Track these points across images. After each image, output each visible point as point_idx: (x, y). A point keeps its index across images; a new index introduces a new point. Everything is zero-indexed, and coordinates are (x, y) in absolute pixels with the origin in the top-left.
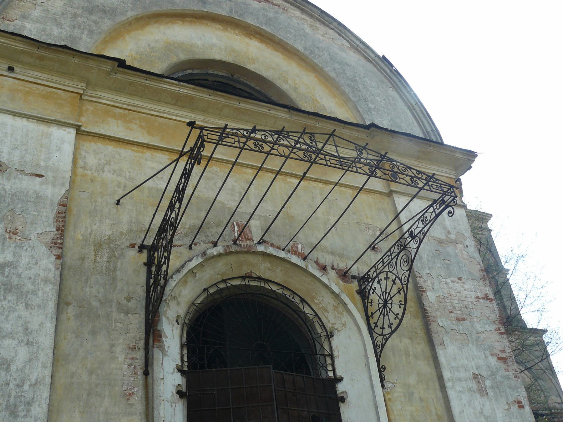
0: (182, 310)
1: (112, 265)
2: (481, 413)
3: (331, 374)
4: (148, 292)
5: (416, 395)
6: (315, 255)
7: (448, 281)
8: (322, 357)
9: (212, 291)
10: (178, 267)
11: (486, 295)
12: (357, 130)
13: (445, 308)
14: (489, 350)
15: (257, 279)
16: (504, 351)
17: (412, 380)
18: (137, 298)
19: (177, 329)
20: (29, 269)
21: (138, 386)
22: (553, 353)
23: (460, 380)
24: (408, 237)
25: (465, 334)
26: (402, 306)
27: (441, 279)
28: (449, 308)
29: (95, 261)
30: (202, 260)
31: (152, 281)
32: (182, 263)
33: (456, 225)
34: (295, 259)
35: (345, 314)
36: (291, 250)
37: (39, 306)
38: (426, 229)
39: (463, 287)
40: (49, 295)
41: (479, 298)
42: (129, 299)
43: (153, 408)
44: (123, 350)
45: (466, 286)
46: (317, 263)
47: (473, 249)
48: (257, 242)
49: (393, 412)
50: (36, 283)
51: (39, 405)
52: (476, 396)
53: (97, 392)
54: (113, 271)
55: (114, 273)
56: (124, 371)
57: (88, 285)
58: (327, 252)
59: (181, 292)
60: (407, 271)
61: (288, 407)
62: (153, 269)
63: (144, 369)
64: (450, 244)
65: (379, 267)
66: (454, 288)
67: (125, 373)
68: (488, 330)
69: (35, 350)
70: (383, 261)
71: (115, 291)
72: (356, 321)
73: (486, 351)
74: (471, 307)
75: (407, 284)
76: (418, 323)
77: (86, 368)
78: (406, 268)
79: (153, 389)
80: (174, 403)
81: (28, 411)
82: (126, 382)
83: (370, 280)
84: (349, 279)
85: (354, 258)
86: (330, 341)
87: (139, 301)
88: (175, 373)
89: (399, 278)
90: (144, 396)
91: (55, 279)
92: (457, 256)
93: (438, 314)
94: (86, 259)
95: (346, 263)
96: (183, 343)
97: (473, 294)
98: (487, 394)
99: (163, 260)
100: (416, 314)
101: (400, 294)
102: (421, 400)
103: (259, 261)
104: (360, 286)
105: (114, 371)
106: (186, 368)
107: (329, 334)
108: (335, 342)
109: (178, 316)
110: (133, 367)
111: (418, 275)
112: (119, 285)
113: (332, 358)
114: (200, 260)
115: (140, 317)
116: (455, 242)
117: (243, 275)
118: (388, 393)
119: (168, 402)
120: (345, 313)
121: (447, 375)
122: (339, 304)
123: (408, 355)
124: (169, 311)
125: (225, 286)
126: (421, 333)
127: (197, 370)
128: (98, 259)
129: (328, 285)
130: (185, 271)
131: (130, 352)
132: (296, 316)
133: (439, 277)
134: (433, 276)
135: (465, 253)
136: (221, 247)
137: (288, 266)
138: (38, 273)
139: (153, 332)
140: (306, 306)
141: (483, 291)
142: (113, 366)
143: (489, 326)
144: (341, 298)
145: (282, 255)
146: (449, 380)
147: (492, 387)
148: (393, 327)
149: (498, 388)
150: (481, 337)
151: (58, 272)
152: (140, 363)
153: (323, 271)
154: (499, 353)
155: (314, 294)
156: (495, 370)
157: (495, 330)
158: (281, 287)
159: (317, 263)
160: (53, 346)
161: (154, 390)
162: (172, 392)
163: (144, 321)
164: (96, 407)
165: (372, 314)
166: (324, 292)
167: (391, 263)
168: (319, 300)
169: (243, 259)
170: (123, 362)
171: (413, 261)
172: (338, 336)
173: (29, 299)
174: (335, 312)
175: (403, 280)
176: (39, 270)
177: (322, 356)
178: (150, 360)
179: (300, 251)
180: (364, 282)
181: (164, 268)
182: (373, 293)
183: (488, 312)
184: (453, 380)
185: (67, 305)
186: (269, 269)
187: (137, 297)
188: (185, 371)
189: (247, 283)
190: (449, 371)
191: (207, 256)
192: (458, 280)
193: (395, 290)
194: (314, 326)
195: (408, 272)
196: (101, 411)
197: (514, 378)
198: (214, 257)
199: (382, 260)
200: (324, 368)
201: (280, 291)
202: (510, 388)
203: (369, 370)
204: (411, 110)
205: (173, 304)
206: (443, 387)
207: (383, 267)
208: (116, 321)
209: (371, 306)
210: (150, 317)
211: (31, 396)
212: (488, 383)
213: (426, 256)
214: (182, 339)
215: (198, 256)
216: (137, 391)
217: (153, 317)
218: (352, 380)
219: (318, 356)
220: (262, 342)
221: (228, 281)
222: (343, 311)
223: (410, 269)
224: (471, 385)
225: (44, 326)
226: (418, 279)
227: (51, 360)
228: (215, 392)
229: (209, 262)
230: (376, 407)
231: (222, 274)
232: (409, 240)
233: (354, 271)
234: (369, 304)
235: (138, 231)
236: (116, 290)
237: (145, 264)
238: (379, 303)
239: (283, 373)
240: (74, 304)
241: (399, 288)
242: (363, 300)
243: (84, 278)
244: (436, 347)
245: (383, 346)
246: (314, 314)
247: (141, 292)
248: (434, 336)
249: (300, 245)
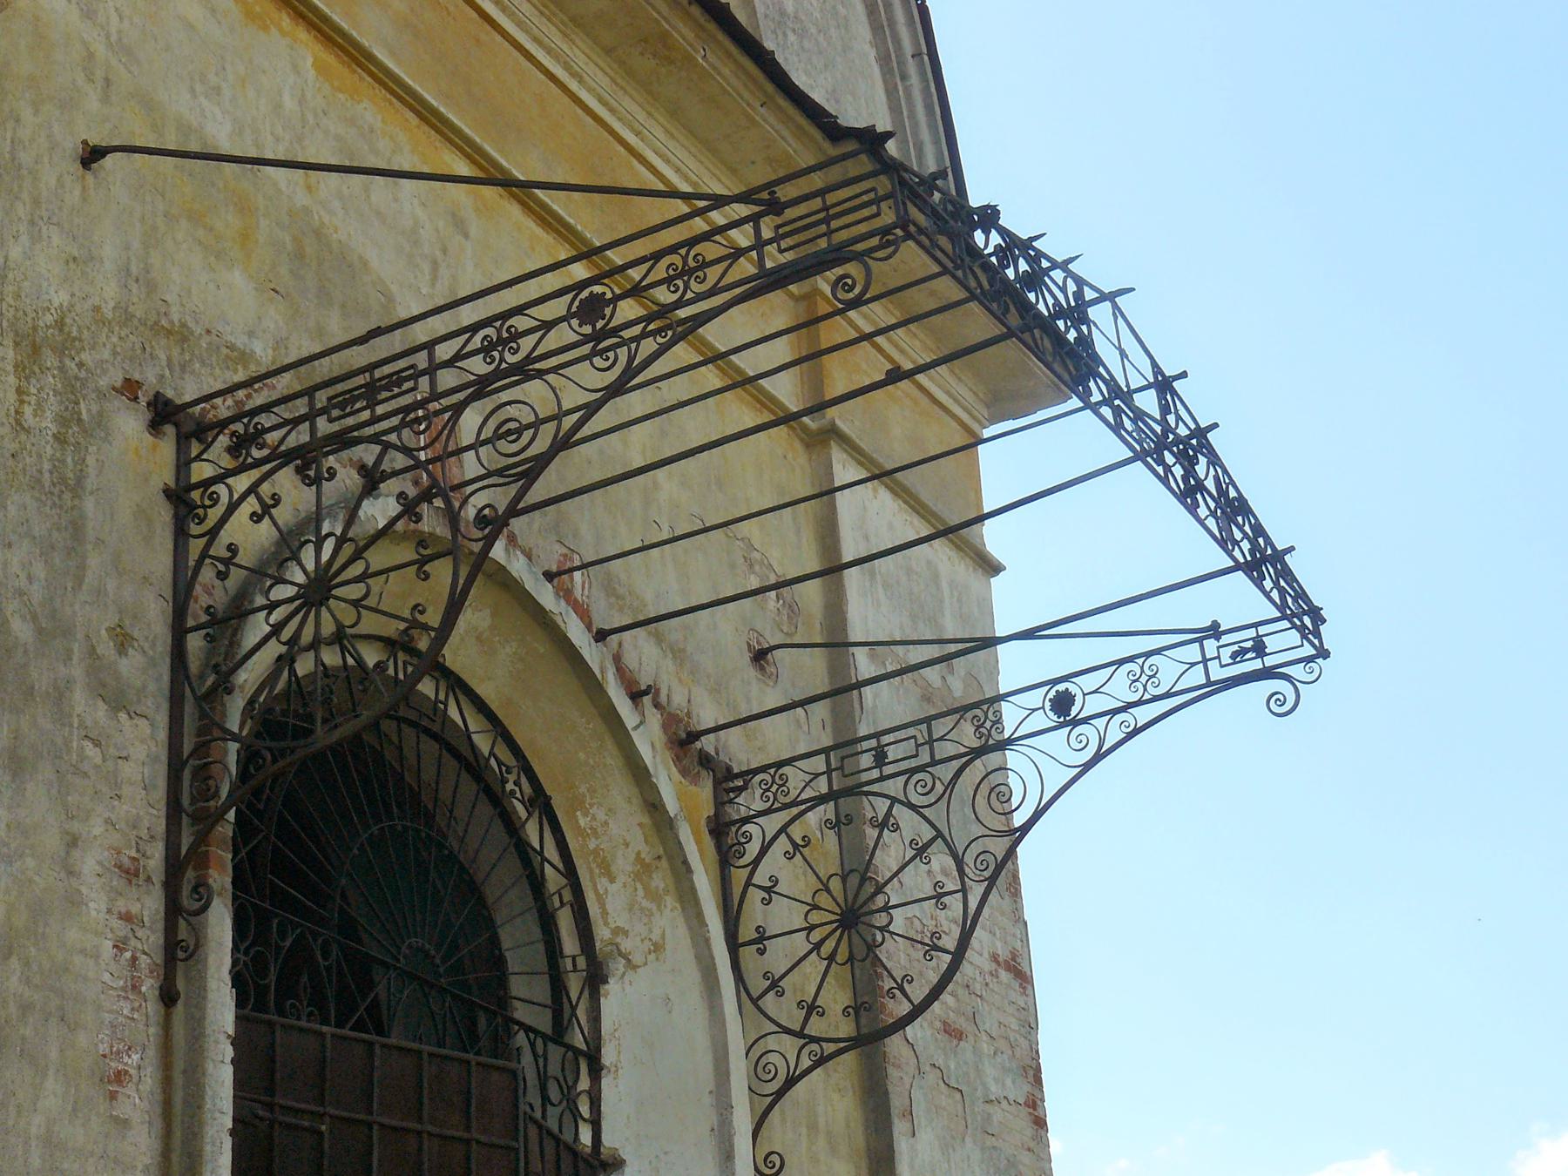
12: (799, 127)
18: (146, 646)
34: (577, 633)
35: (669, 907)
42: (123, 640)
63: (162, 972)
71: (80, 586)
72: (710, 949)
90: (159, 1097)
95: (690, 691)
110: (128, 955)
113: (596, 1070)
120: (670, 901)
122: (659, 857)
129: (651, 770)
137: (542, 646)
144: (677, 837)
155: (583, 789)
166: (620, 792)
168: (594, 818)
172: (627, 987)
174: (639, 886)
196: (34, 1130)
204: (891, 71)
222: (667, 892)
228: (323, 1128)
235: (149, 323)
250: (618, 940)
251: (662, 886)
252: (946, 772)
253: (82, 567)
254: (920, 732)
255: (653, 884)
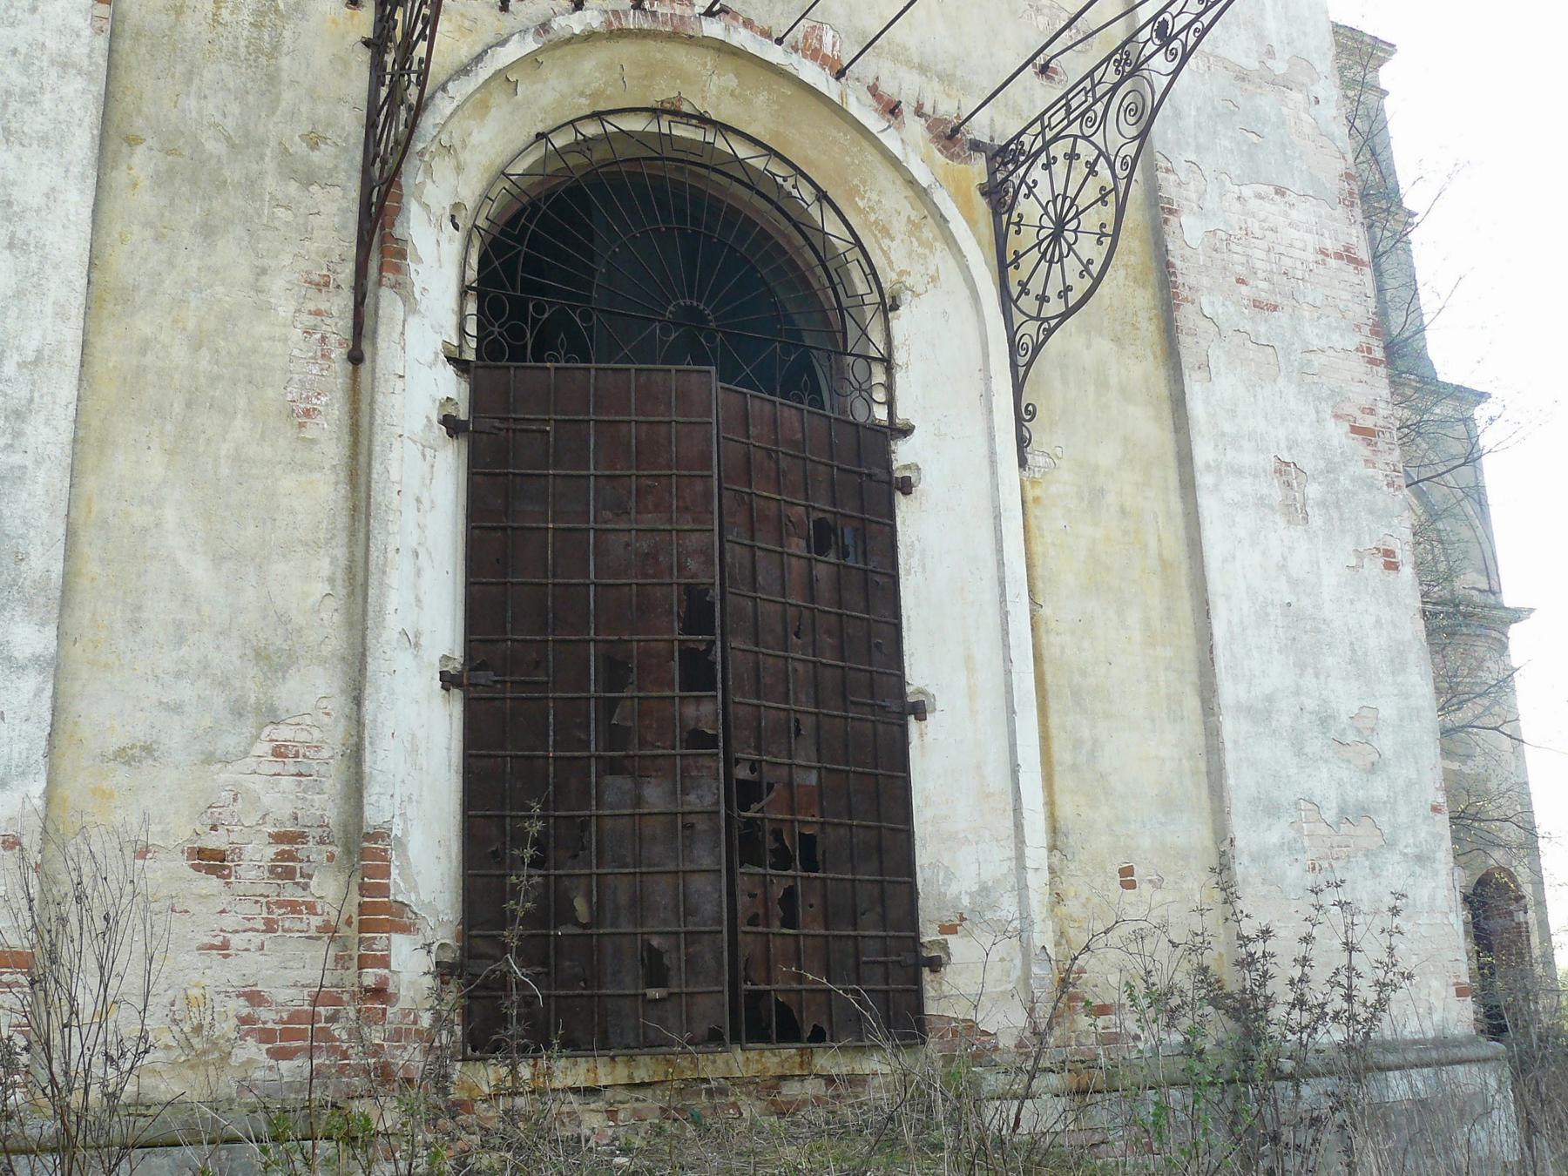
0: (469, 190)
1: (266, 37)
2: (1283, 567)
3: (881, 414)
4: (371, 124)
5: (1111, 498)
6: (868, 67)
7: (1247, 191)
8: (861, 362)
9: (560, 141)
10: (465, 61)
11: (1347, 249)
13: (1225, 268)
14: (1331, 403)
15: (694, 122)
16: (1372, 411)
17: (1107, 455)
18: (339, 141)
19: (450, 240)
20: (12, 25)
21: (331, 392)
22: (1500, 446)
23: (1238, 472)
24: (1151, 38)
25: (1271, 349)
26: (1107, 241)
27: (1228, 183)
28: (1239, 268)
29: (216, 20)
30: (535, 46)
31: (384, 92)
32: (478, 49)
33: (1295, 35)
36: (801, 45)
37: (44, 139)
38: (1206, 19)
39: (1286, 215)
40: (75, 108)
41: (1327, 255)
42: (314, 140)
43: (370, 455)
44: (289, 287)
45: (1294, 214)
46: (873, 90)
47: (1334, 112)
48: (703, 10)
49: (1043, 536)
50: (35, 68)
51: (47, 422)
52: (1274, 522)
53: (213, 398)
54: (270, 56)
55: (273, 61)
56: (292, 345)
57: (194, 88)
58: (909, 63)
59: (470, 134)
60: (1134, 139)
61: (750, 487)
62: (389, 58)
63: (351, 344)
64: (1268, 88)
65: (1054, 122)
66: (1262, 215)
67: (296, 352)
68: (1338, 347)
69: (34, 265)
70: (1067, 105)
71: (273, 113)
73: (1324, 403)
74: (1299, 274)
75: (1129, 177)
76: (1143, 300)
77: (184, 329)
78: (1132, 131)
79: (372, 402)
80: (431, 447)
81: (17, 434)
82: (296, 377)
83: (1022, 158)
84: (962, 149)
85: (983, 89)
86: (887, 320)
87: (346, 150)
88: (440, 365)
89: (1108, 160)
90: (346, 420)
91: (91, 64)
92: (1284, 123)
93: (1205, 281)
94: (189, 12)
96: (467, 283)
97: (1312, 241)
98: (1306, 519)
99: (420, 26)
100: (1141, 273)
101: (1106, 204)
102: (1123, 511)
103: (705, 65)
104: (992, 173)
105: (264, 344)
106: (470, 356)
107: (888, 301)
108: (901, 324)
109: (457, 206)
110: (318, 336)
111: (1162, 163)
112: (287, 96)
114: (531, 45)
115: (343, 197)
116: (1283, 84)
117: (655, 106)
118: (1034, 482)
119: (415, 442)
120: (939, 245)
121: (1203, 452)
123: (1102, 385)
124: (429, 185)
125: (600, 131)
126: (1149, 329)
127: (503, 363)
128: (225, 14)
130: (484, 72)
131: (312, 292)
132: (800, 241)
133: (1224, 177)
134: (1206, 174)
135: (1304, 116)
136: (596, 13)
138: (41, 39)
139: (382, 241)
140: (830, 214)
141: (1341, 237)
142: (261, 329)
143: (1342, 336)
145: (775, 54)
146: (1208, 467)
147: (1323, 504)
148: (1073, 298)
149: (1338, 506)
150: (1316, 363)
151: (101, 43)
152: (339, 325)
153: (890, 116)
154: (1358, 414)
155: (856, 182)
156: (1336, 460)
157: (1357, 349)
158: (765, 152)
159: (873, 90)
160: (87, 260)
161: (376, 406)
162: (427, 417)
163: (356, 208)
164: (209, 440)
165: (1018, 256)
166: (884, 176)
167: (1091, 114)
168: (869, 199)
169: (658, 56)
170: (289, 322)
171: (1155, 111)
172: (914, 309)
173: (15, 115)
174: (913, 239)
175: (1118, 165)
176: (44, 29)
177: (860, 360)
178: (368, 323)
179: (827, 50)
180: (1005, 165)
181: (421, 49)
182: (1027, 196)
183: (1345, 295)
184: (1218, 468)
185: (130, 145)
186: (732, 94)
187: (340, 137)
188: (468, 362)
189: (665, 130)
190: (1213, 445)
191: (551, 36)
192: (1276, 193)
193: (1090, 193)
194: (848, 273)
195: (1137, 142)
196: (223, 453)
197: (1385, 488)
198: (571, 40)
199: (1064, 102)
200: (864, 394)
201: (759, 163)
202: (1371, 512)
203: (990, 411)
205: (442, 167)
206: (1188, 486)
207: (1066, 122)
208: (274, 203)
209: (1018, 232)
210: (374, 200)
211: (24, 393)
212: (1314, 491)
213: (1193, 113)
214: (464, 272)
215: (525, 31)
216: (327, 405)
217: (383, 197)
218: (938, 435)
219: (850, 359)
220: (695, 304)
221: (610, 118)
223: (1143, 135)
224: (1265, 491)
225: (62, 198)
226: (1160, 175)
227: (81, 299)
229: (558, 53)
230: (997, 517)
231: (594, 96)
232: (1151, 48)
233: (980, 128)
234: (1013, 228)
236: (278, 113)
237: (367, 43)
238: (1042, 227)
239: (745, 394)
240: (150, 142)
241: (1103, 188)
242: (996, 214)
243: (180, 68)
244: (1186, 372)
245: (1037, 348)
246: (852, 240)
247: (351, 123)
248: (1185, 341)
249: (831, 33)
250: (903, 279)
251: (931, 235)
252: (1099, 108)
253: (277, 100)
254: (1087, 84)
255: (924, 236)
